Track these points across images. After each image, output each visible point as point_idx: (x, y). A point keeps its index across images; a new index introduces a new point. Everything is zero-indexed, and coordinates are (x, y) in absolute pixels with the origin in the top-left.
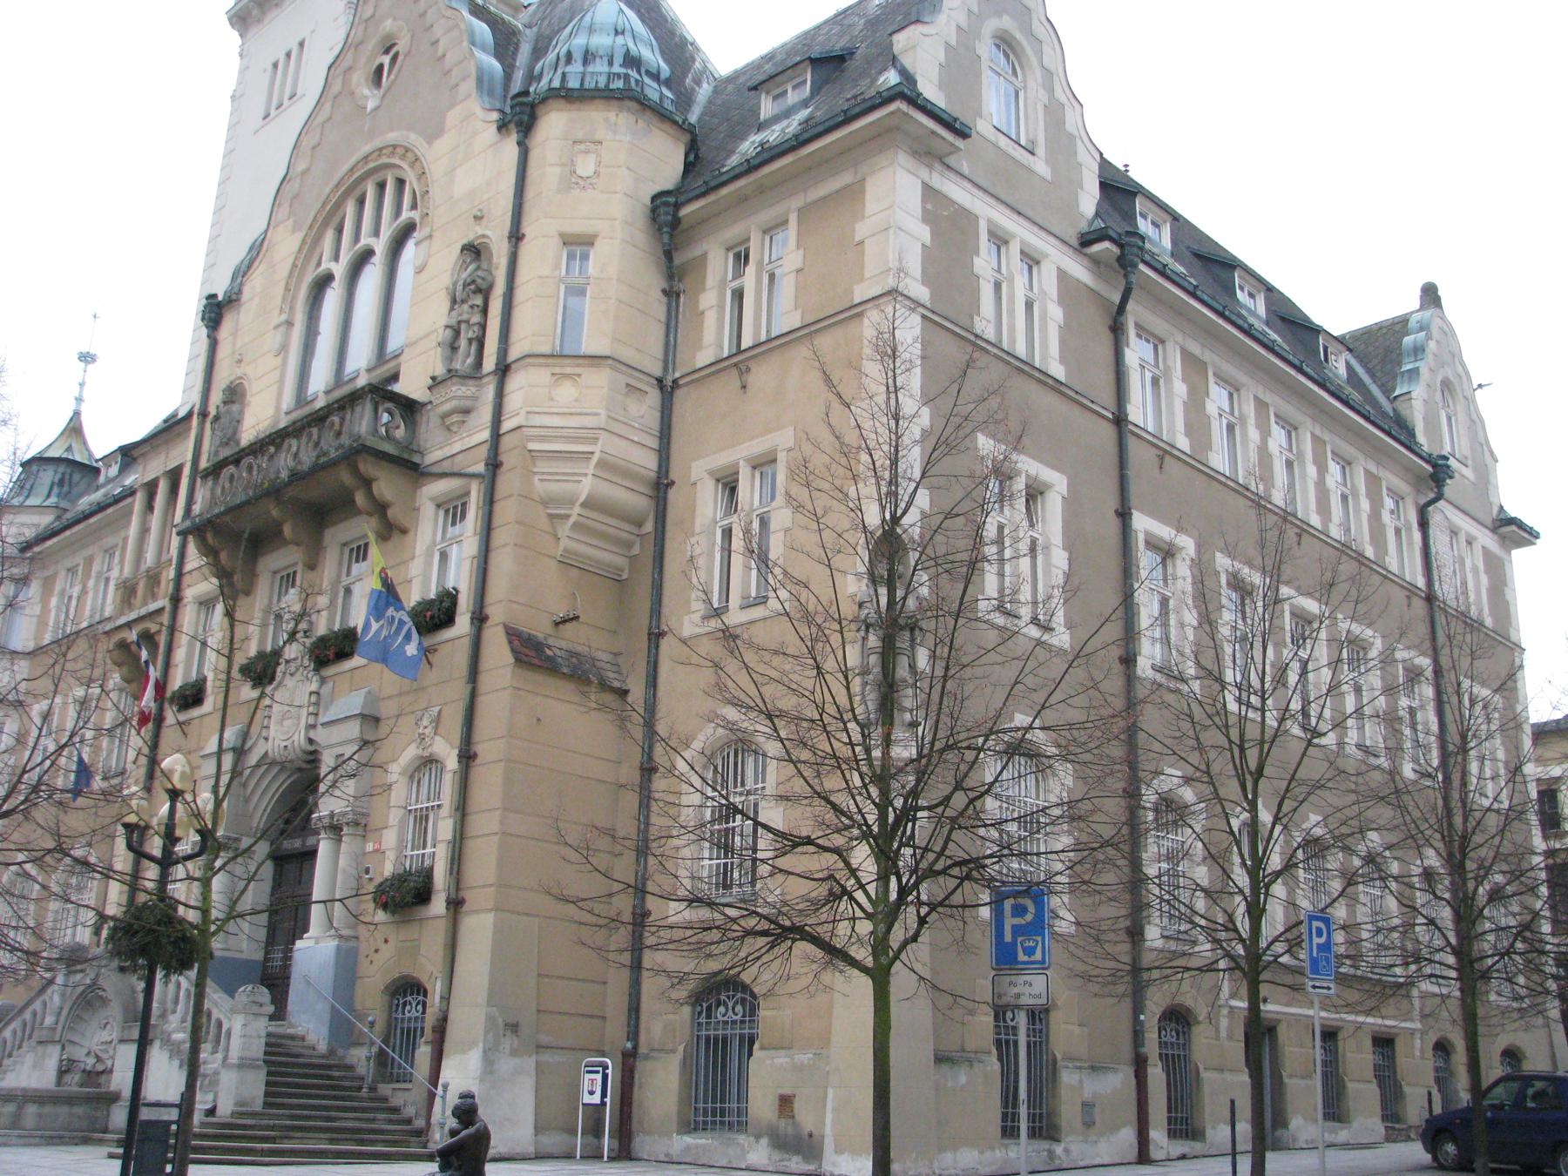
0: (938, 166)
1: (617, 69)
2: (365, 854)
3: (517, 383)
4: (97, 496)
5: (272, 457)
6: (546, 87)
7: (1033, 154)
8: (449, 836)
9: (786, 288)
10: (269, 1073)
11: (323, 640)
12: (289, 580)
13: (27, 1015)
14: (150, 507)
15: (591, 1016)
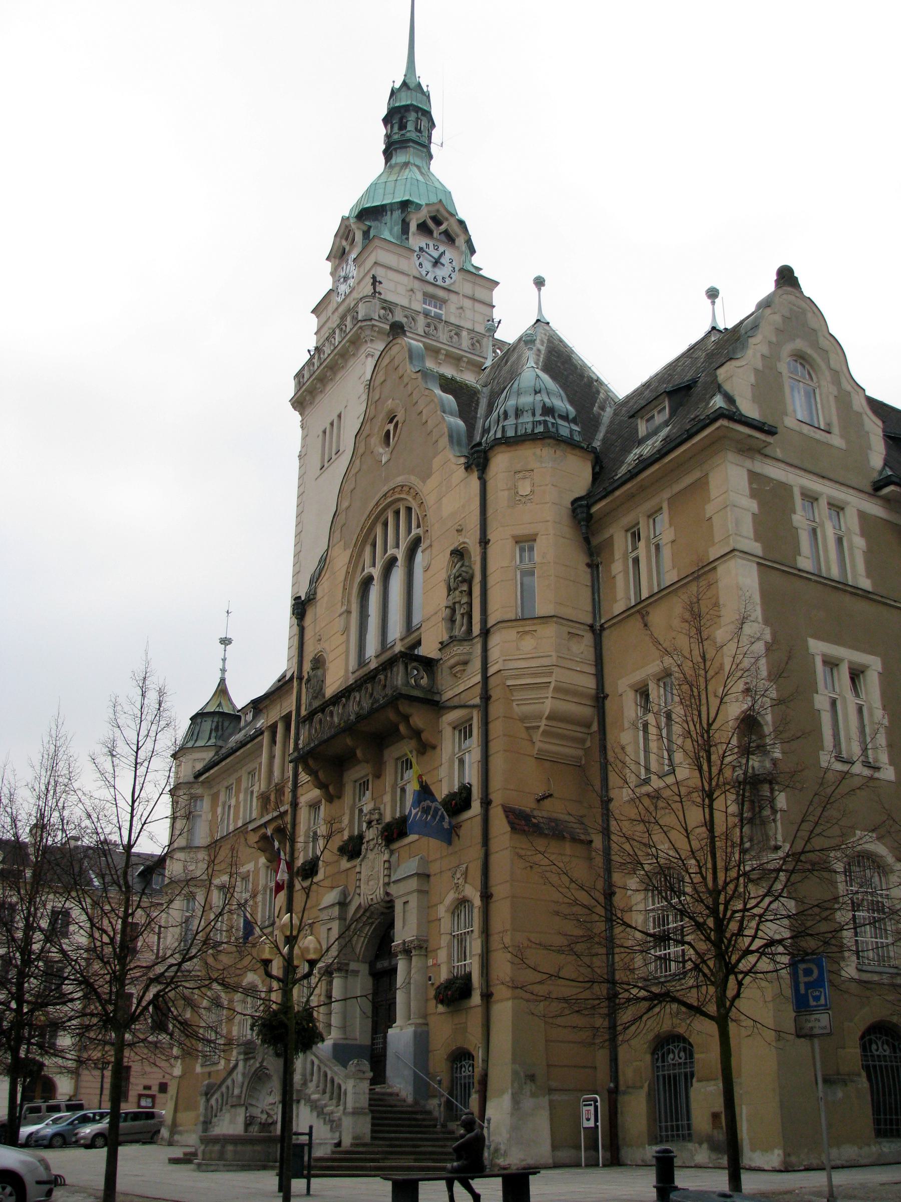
0: (758, 456)
1: (538, 418)
2: (428, 967)
3: (495, 640)
4: (239, 736)
5: (344, 706)
6: (493, 438)
7: (829, 433)
8: (479, 951)
9: (667, 553)
10: (373, 1118)
11: (389, 825)
12: (364, 786)
13: (224, 1089)
14: (273, 741)
15: (585, 1067)
